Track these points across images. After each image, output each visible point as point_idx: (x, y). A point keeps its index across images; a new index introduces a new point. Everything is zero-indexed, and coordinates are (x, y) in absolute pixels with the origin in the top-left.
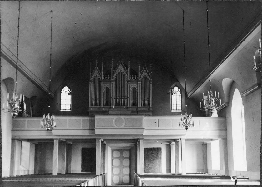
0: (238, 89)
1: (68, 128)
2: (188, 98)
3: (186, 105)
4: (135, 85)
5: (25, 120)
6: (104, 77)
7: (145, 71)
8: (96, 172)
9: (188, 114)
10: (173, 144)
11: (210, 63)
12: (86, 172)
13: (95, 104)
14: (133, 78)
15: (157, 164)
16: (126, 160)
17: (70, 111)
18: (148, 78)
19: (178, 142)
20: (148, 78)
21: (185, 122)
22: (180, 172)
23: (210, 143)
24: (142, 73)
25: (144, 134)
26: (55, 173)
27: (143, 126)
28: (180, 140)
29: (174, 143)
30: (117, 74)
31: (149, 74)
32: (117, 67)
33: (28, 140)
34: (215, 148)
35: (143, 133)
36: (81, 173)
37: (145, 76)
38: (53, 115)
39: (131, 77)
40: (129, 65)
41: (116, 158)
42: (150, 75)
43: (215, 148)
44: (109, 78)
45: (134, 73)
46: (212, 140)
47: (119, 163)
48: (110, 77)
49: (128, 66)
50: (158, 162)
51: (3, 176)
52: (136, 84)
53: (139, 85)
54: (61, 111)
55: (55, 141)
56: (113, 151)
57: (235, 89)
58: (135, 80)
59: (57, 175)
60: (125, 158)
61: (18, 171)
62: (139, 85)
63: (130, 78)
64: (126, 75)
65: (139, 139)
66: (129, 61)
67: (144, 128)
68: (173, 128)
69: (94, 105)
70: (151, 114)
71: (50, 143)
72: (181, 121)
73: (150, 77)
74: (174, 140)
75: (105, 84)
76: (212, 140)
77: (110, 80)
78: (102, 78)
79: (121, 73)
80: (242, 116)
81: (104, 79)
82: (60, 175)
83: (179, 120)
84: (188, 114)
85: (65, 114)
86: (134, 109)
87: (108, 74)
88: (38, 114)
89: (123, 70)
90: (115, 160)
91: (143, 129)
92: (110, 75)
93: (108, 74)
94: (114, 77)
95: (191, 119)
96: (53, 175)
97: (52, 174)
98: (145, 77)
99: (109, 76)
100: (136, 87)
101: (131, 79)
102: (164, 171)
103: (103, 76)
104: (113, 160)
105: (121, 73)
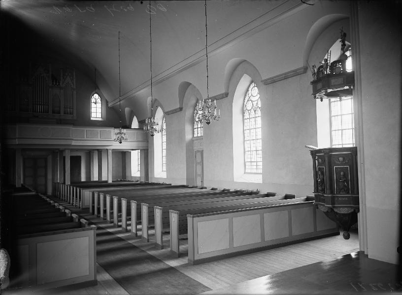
14: (55, 83)
34: (135, 158)
39: (53, 82)
43: (135, 158)
44: (58, 84)
54: (92, 119)
68: (101, 139)
101: (53, 84)
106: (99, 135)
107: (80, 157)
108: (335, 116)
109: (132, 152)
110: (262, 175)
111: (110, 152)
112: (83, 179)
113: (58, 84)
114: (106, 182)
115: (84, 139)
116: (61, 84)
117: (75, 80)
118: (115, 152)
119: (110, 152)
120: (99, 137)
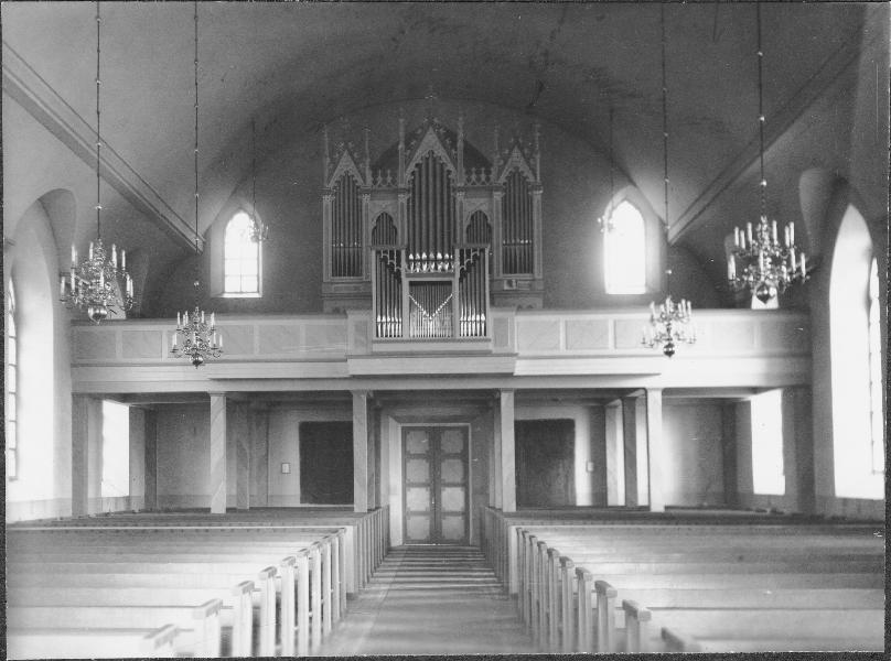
0: (858, 208)
1: (256, 355)
2: (668, 244)
3: (668, 268)
4: (482, 200)
5: (161, 332)
6: (375, 175)
7: (345, 154)
8: (352, 502)
9: (676, 301)
10: (616, 407)
11: (763, 119)
12: (316, 503)
13: (349, 268)
14: (474, 177)
15: (558, 475)
16: (451, 461)
17: (257, 296)
18: (527, 177)
19: (635, 399)
20: (527, 177)
21: (664, 331)
22: (642, 501)
23: (749, 403)
24: (335, 163)
25: (517, 373)
26: (218, 505)
27: (513, 346)
28: (642, 392)
29: (618, 402)
30: (417, 165)
31: (532, 161)
32: (420, 139)
33: (123, 398)
34: (767, 421)
35: (514, 367)
36: (299, 505)
37: (517, 168)
38: (213, 315)
39: (468, 173)
40: (461, 135)
41: (418, 456)
42: (535, 165)
43: (767, 421)
44: (389, 179)
45: (475, 160)
46: (755, 390)
47: (427, 474)
48: (394, 175)
49: (456, 135)
50: (561, 470)
51: (12, 516)
52: (486, 199)
53: (402, 204)
54: (226, 296)
55: (214, 400)
56: (405, 432)
57: (842, 213)
58: (389, 186)
59: (223, 511)
60: (449, 456)
61: (96, 499)
62: (402, 204)
63: (465, 177)
64: (450, 167)
65: (498, 391)
66: (401, 120)
67: (516, 351)
68: (618, 352)
69: (340, 271)
70: (539, 302)
71: (197, 403)
72: (652, 330)
73: (535, 175)
74: (623, 393)
75: (473, 200)
76: (755, 390)
77: (394, 187)
78: (365, 181)
79: (430, 161)
80: (869, 302)
81: (375, 182)
82: (141, 511)
83: (643, 323)
84: (676, 301)
85: (240, 308)
86: (345, 284)
87: (385, 163)
88: (169, 315)
89: (440, 152)
90: (412, 464)
91: (516, 355)
92: (395, 165)
93: (385, 163)
94: (405, 176)
95: (685, 320)
96: (212, 511)
97: (209, 509)
98: (347, 178)
99: (389, 172)
100: (484, 208)
101: (469, 180)
102: (582, 494)
103: (368, 173)
104: (408, 464)
105: (430, 161)
106: (611, 335)
107: (567, 427)
108: (98, 8)
109: (754, 400)
110: (215, 654)
111: (655, 400)
112: (582, 494)
113: (389, 179)
114: (647, 508)
115: (556, 353)
116: (492, 176)
117: (538, 156)
118: (677, 399)
119: (655, 400)
120: (611, 343)
